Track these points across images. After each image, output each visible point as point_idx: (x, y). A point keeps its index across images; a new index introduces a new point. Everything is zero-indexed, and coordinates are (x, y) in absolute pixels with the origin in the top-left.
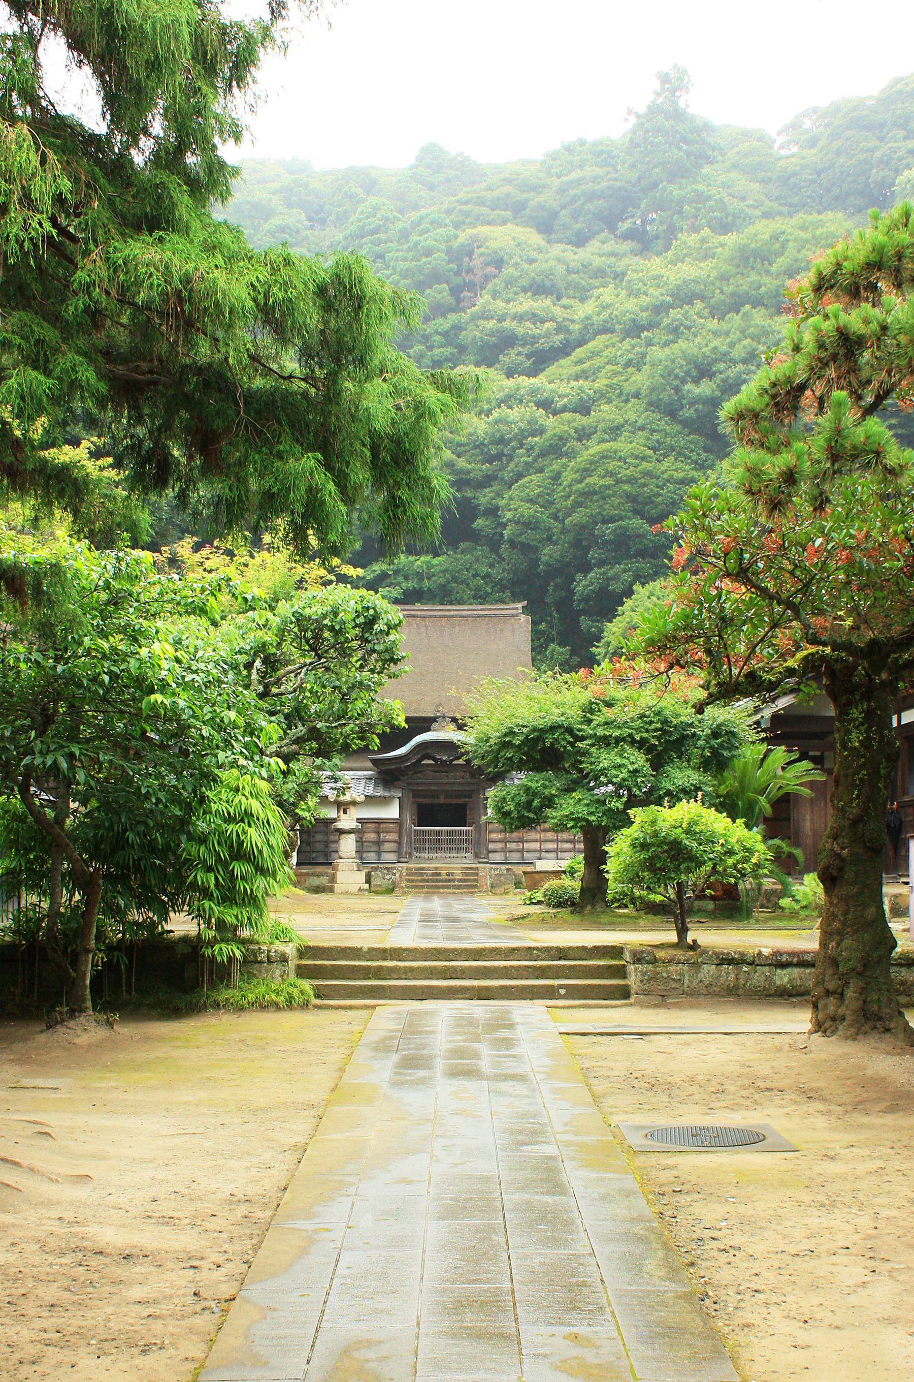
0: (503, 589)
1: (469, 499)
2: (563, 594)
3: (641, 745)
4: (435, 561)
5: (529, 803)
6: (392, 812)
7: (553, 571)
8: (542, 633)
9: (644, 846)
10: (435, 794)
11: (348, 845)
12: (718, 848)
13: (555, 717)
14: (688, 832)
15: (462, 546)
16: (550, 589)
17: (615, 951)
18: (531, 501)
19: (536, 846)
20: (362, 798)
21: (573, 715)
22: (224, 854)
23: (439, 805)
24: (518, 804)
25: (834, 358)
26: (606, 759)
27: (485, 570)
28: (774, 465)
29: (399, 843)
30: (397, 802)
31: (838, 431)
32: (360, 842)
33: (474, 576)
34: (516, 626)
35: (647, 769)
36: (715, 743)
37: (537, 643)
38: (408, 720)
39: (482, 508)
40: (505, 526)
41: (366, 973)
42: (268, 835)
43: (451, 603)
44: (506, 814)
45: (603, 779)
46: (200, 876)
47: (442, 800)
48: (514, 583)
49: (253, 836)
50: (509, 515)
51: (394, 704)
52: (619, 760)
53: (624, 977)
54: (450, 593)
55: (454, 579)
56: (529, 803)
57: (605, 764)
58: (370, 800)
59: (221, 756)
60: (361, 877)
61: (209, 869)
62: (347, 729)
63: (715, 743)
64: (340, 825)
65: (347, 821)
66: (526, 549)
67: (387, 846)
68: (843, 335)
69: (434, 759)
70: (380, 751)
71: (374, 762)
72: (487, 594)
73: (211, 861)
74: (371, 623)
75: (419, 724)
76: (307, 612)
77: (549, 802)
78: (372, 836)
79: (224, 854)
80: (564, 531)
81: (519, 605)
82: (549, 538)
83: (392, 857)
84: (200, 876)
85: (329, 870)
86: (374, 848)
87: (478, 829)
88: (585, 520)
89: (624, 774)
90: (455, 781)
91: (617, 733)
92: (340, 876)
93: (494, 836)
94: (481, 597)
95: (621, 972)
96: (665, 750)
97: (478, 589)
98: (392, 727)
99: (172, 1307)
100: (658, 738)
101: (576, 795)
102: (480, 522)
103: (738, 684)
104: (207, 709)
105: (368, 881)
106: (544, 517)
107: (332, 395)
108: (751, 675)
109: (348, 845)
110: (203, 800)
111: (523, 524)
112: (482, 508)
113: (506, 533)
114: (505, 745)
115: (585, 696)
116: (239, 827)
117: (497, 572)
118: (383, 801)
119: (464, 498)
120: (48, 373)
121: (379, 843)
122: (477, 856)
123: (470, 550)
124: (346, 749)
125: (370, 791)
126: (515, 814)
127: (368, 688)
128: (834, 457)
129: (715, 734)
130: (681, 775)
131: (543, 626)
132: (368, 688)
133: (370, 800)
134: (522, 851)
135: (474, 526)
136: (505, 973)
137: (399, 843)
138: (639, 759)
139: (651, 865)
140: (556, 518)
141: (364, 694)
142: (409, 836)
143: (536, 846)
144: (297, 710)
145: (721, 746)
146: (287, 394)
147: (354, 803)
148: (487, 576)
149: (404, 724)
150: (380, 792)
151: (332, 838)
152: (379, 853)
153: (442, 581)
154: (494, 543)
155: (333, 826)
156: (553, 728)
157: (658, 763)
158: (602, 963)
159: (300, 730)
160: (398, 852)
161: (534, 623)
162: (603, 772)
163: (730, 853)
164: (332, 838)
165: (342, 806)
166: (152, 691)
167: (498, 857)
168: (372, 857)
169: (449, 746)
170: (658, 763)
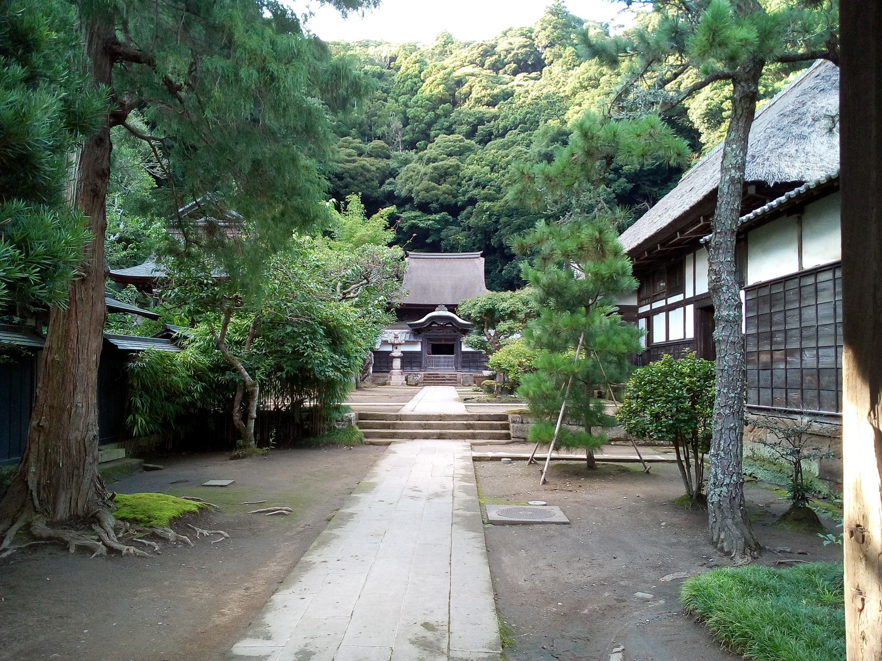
11: (397, 363)
17: (504, 417)
41: (388, 426)
47: (443, 342)
53: (509, 429)
58: (407, 343)
64: (393, 354)
65: (397, 353)
90: (448, 333)
95: (507, 427)
99: (131, 531)
105: (406, 380)
109: (397, 363)
136: (454, 427)
147: (400, 344)
158: (399, 431)
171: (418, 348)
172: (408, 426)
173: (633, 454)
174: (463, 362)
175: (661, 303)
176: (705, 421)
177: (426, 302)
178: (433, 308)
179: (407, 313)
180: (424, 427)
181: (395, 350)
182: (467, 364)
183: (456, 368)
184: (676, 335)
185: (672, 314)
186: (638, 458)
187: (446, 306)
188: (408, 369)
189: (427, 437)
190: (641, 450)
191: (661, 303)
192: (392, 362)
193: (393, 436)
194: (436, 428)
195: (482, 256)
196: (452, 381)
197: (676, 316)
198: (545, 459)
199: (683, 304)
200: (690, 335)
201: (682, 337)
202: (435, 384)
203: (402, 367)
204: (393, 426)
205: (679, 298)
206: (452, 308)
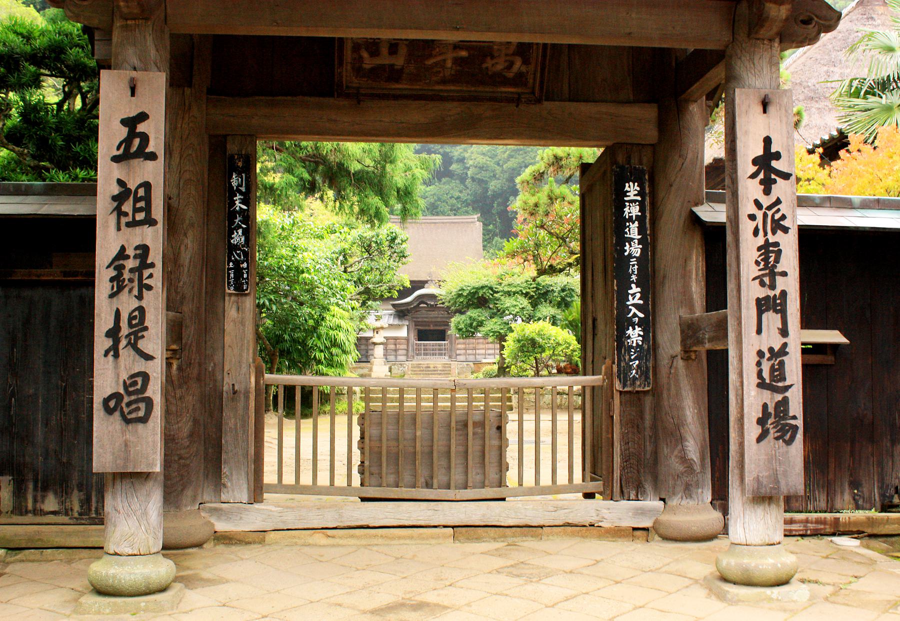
0: (468, 205)
1: (448, 153)
2: (502, 208)
3: (526, 295)
4: (428, 189)
5: (471, 324)
6: (403, 333)
7: (496, 196)
8: (489, 231)
9: (519, 341)
10: (428, 324)
12: (552, 341)
13: (484, 282)
14: (539, 334)
15: (444, 180)
16: (495, 205)
18: (484, 154)
19: (483, 352)
20: (387, 326)
21: (492, 281)
22: (328, 344)
23: (430, 330)
24: (466, 325)
25: (553, 164)
26: (508, 302)
27: (457, 194)
28: (532, 200)
29: (407, 350)
30: (406, 328)
31: (551, 191)
32: (386, 349)
33: (451, 198)
34: (472, 228)
35: (529, 307)
36: (563, 294)
37: (487, 237)
38: (411, 282)
39: (455, 158)
40: (468, 168)
42: (347, 338)
43: (438, 214)
44: (460, 330)
45: (507, 312)
46: (318, 354)
47: (432, 328)
48: (474, 202)
49: (341, 336)
50: (471, 162)
51: (403, 276)
52: (515, 303)
54: (437, 207)
55: (439, 199)
56: (471, 324)
57: (508, 305)
58: (391, 326)
59: (332, 300)
60: (387, 368)
61: (322, 351)
62: (382, 288)
63: (563, 294)
65: (378, 338)
66: (481, 182)
67: (400, 352)
68: (556, 157)
69: (426, 304)
70: (398, 299)
71: (394, 305)
72: (459, 208)
73: (322, 348)
74: (393, 240)
75: (418, 284)
76: (365, 235)
77: (481, 324)
78: (392, 347)
79: (328, 344)
80: (503, 172)
81: (476, 216)
82: (494, 176)
83: (403, 358)
84: (318, 354)
85: (368, 365)
86: (393, 353)
87: (451, 343)
88: (515, 165)
89: (518, 310)
91: (514, 290)
92: (375, 368)
93: (459, 346)
94: (455, 211)
96: (538, 298)
97: (453, 205)
98: (404, 287)
100: (535, 292)
101: (494, 320)
102: (454, 167)
103: (545, 269)
104: (326, 280)
105: (390, 371)
106: (491, 164)
107: (383, 174)
108: (551, 266)
109: (379, 351)
110: (323, 319)
111: (480, 168)
112: (455, 158)
113: (469, 173)
114: (460, 295)
115: (499, 271)
116: (335, 332)
117: (464, 196)
118: (399, 327)
119: (445, 152)
120: (293, 175)
121: (396, 350)
122: (450, 357)
123: (448, 183)
124: (381, 298)
125: (391, 321)
126: (464, 330)
127: (393, 269)
128: (551, 199)
129: (563, 290)
130: (546, 310)
131: (491, 227)
132: (393, 269)
133: (391, 326)
134: (475, 355)
135: (451, 168)
137: (407, 350)
138: (525, 302)
139: (522, 349)
140: (498, 164)
141: (391, 272)
142: (413, 346)
143: (483, 352)
144: (359, 279)
145: (566, 296)
146: (368, 173)
147: (382, 328)
148: (458, 198)
149: (409, 286)
150: (397, 322)
151: (370, 347)
152: (396, 356)
153: (432, 200)
154: (463, 179)
155: (371, 341)
156: (482, 287)
157: (534, 305)
159: (361, 289)
160: (407, 355)
161: (485, 225)
162: (507, 308)
163: (558, 344)
164: (370, 347)
165: (376, 330)
166: (303, 272)
167: (462, 358)
168: (392, 358)
169: (433, 297)
170: (534, 305)
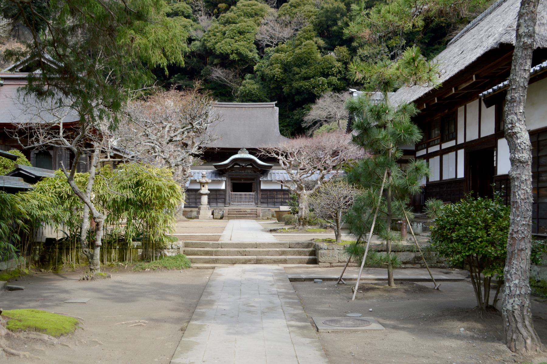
11: (205, 200)
47: (243, 181)
64: (202, 192)
90: (249, 173)
105: (213, 214)
109: (205, 200)
136: (268, 253)
171: (223, 187)
172: (228, 253)
173: (426, 275)
174: (262, 198)
175: (436, 148)
176: (458, 214)
177: (227, 146)
178: (235, 151)
179: (210, 156)
180: (241, 253)
181: (203, 188)
182: (265, 201)
183: (257, 204)
184: (448, 175)
185: (445, 157)
186: (428, 277)
187: (247, 149)
188: (214, 205)
189: (245, 262)
190: (432, 271)
191: (436, 148)
192: (200, 198)
193: (215, 261)
194: (247, 254)
195: (276, 105)
196: (256, 216)
197: (449, 158)
198: (356, 279)
199: (456, 148)
200: (461, 174)
201: (454, 177)
202: (237, 218)
203: (209, 203)
204: (216, 253)
205: (452, 143)
206: (252, 151)
